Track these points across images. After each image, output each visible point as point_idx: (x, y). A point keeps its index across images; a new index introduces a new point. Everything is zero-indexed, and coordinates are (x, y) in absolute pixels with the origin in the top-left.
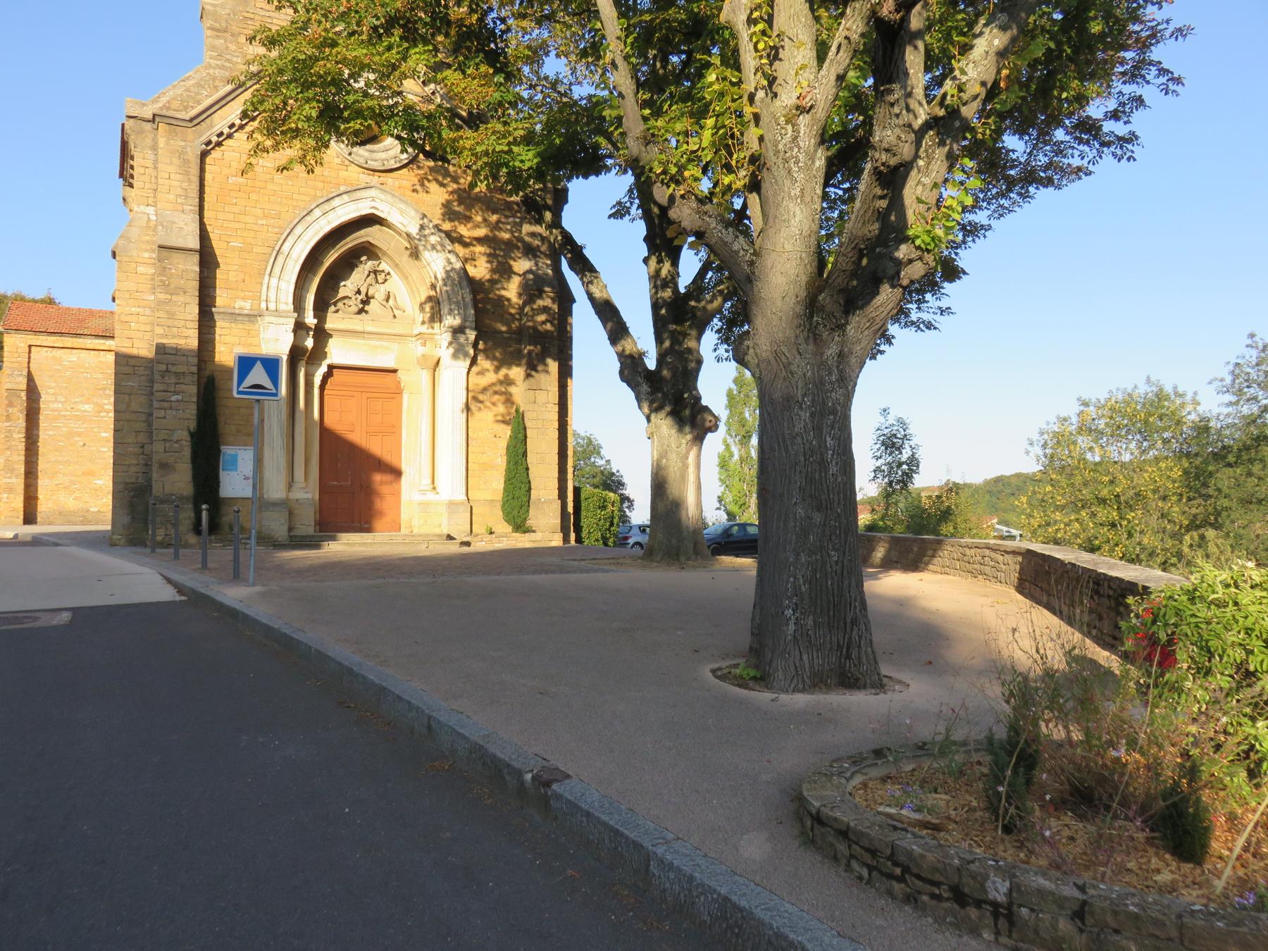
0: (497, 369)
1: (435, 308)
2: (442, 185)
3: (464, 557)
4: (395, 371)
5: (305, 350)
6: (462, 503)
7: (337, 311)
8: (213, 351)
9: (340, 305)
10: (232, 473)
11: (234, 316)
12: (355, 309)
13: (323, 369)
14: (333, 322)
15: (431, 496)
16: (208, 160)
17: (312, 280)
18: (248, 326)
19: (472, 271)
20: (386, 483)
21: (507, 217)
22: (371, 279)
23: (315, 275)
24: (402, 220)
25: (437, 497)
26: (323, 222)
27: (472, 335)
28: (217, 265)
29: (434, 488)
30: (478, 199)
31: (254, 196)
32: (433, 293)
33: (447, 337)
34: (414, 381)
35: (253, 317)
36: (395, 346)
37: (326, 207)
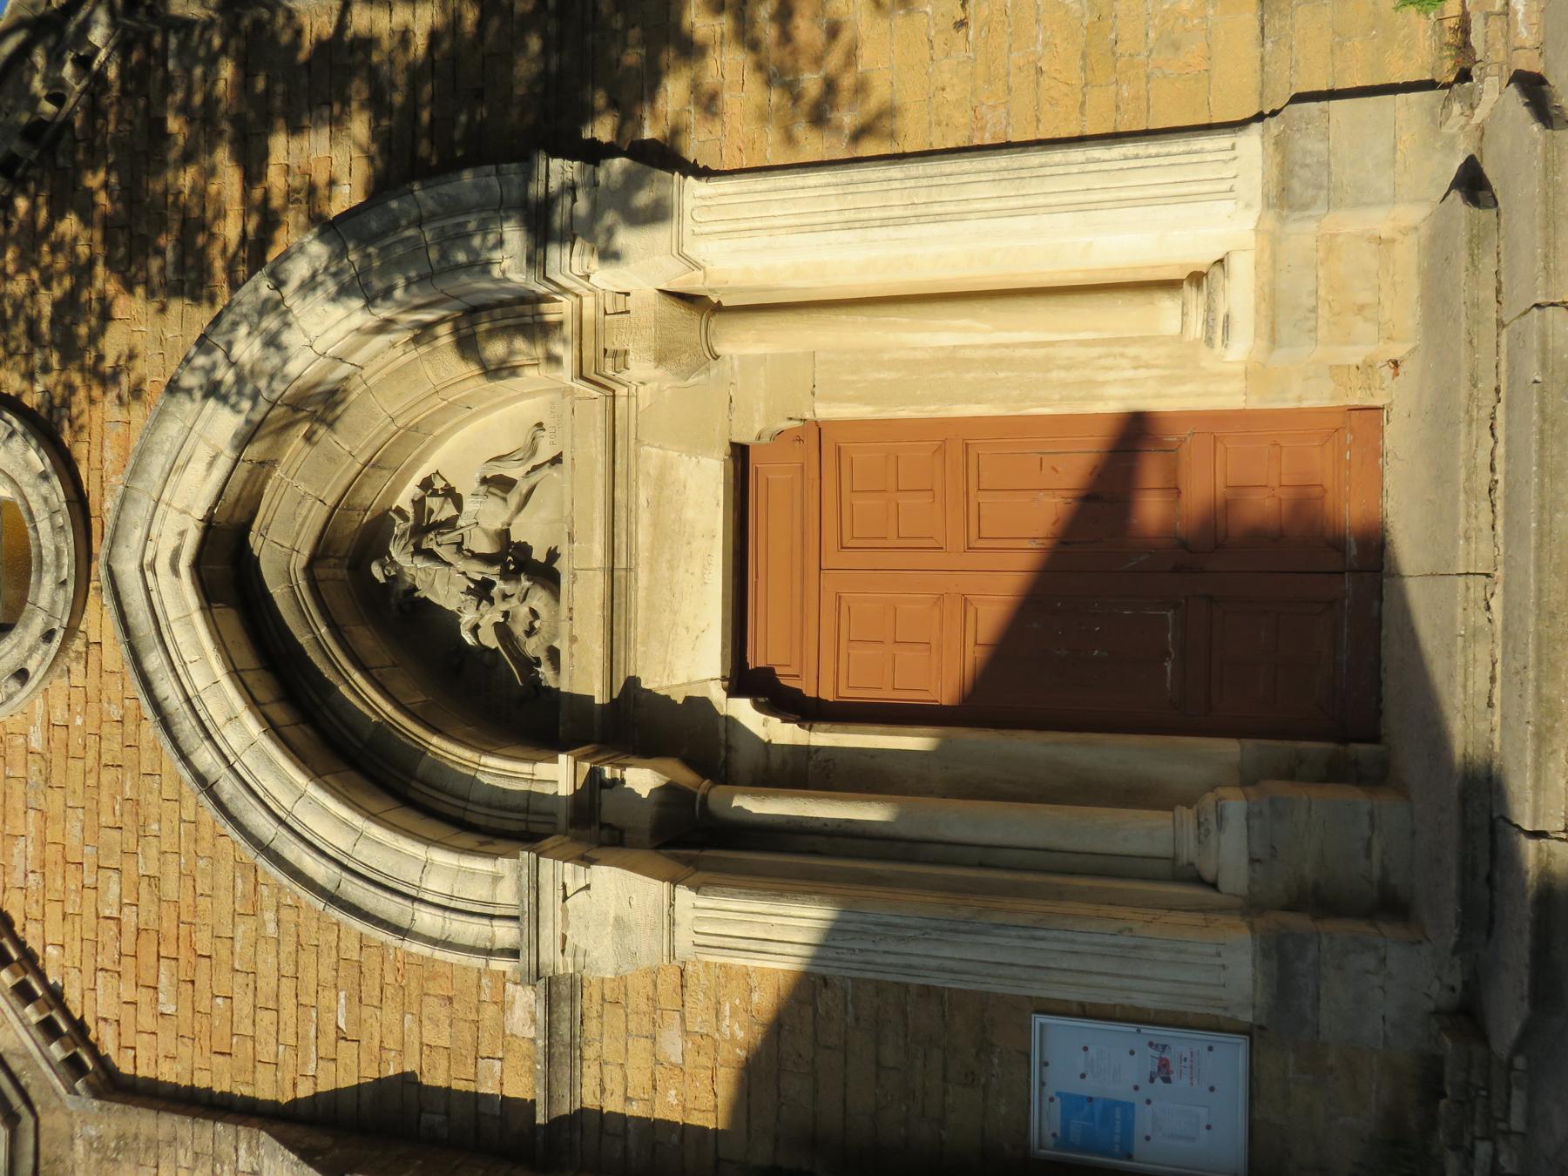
0: (691, 50)
1: (496, 325)
2: (106, 316)
3: (57, 471)
4: (740, 454)
5: (669, 794)
6: (1280, 143)
7: (554, 655)
8: (684, 1129)
9: (532, 647)
10: (1144, 1121)
11: (559, 1049)
12: (539, 599)
13: (743, 711)
14: (584, 677)
15: (1239, 294)
16: (142, 1059)
17: (439, 766)
18: (590, 1003)
19: (346, 197)
20: (1174, 490)
21: (167, 85)
22: (442, 545)
23: (421, 752)
24: (197, 467)
25: (1242, 267)
26: (233, 739)
27: (560, 170)
28: (407, 1080)
29: (1197, 278)
30: (130, 194)
31: (203, 943)
32: (444, 330)
33: (570, 264)
34: (761, 382)
35: (558, 993)
36: (652, 455)
37: (186, 727)
